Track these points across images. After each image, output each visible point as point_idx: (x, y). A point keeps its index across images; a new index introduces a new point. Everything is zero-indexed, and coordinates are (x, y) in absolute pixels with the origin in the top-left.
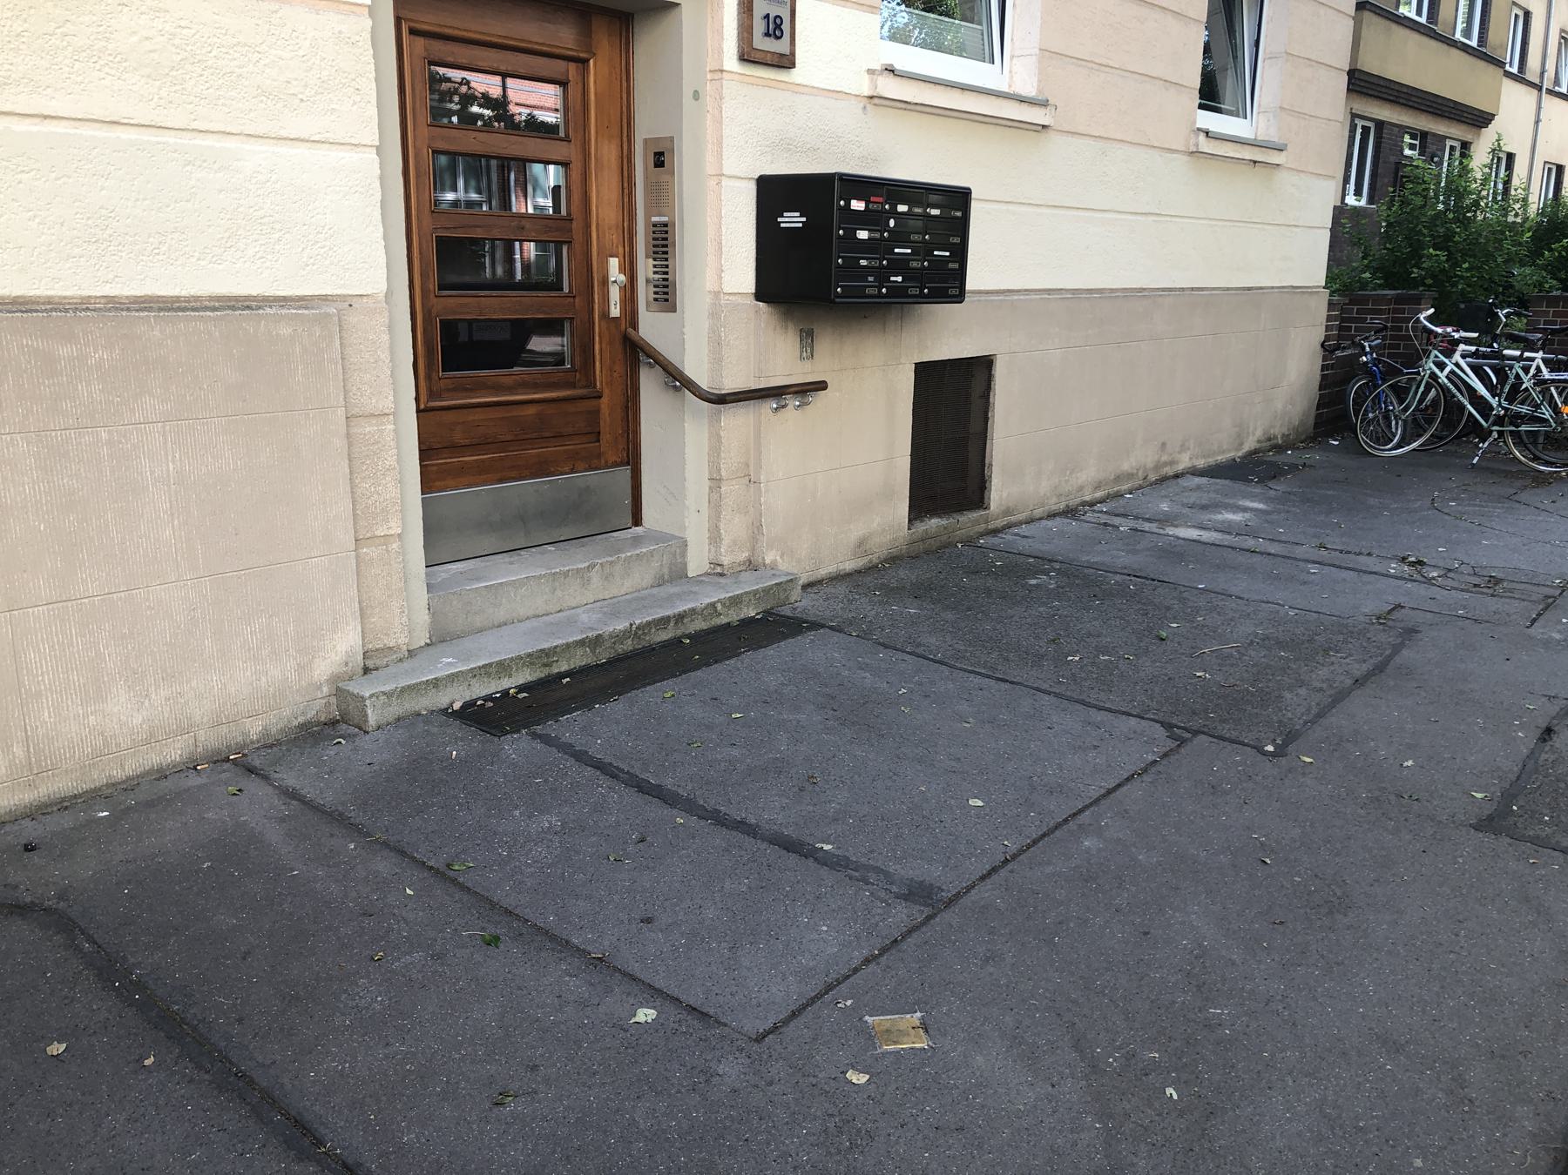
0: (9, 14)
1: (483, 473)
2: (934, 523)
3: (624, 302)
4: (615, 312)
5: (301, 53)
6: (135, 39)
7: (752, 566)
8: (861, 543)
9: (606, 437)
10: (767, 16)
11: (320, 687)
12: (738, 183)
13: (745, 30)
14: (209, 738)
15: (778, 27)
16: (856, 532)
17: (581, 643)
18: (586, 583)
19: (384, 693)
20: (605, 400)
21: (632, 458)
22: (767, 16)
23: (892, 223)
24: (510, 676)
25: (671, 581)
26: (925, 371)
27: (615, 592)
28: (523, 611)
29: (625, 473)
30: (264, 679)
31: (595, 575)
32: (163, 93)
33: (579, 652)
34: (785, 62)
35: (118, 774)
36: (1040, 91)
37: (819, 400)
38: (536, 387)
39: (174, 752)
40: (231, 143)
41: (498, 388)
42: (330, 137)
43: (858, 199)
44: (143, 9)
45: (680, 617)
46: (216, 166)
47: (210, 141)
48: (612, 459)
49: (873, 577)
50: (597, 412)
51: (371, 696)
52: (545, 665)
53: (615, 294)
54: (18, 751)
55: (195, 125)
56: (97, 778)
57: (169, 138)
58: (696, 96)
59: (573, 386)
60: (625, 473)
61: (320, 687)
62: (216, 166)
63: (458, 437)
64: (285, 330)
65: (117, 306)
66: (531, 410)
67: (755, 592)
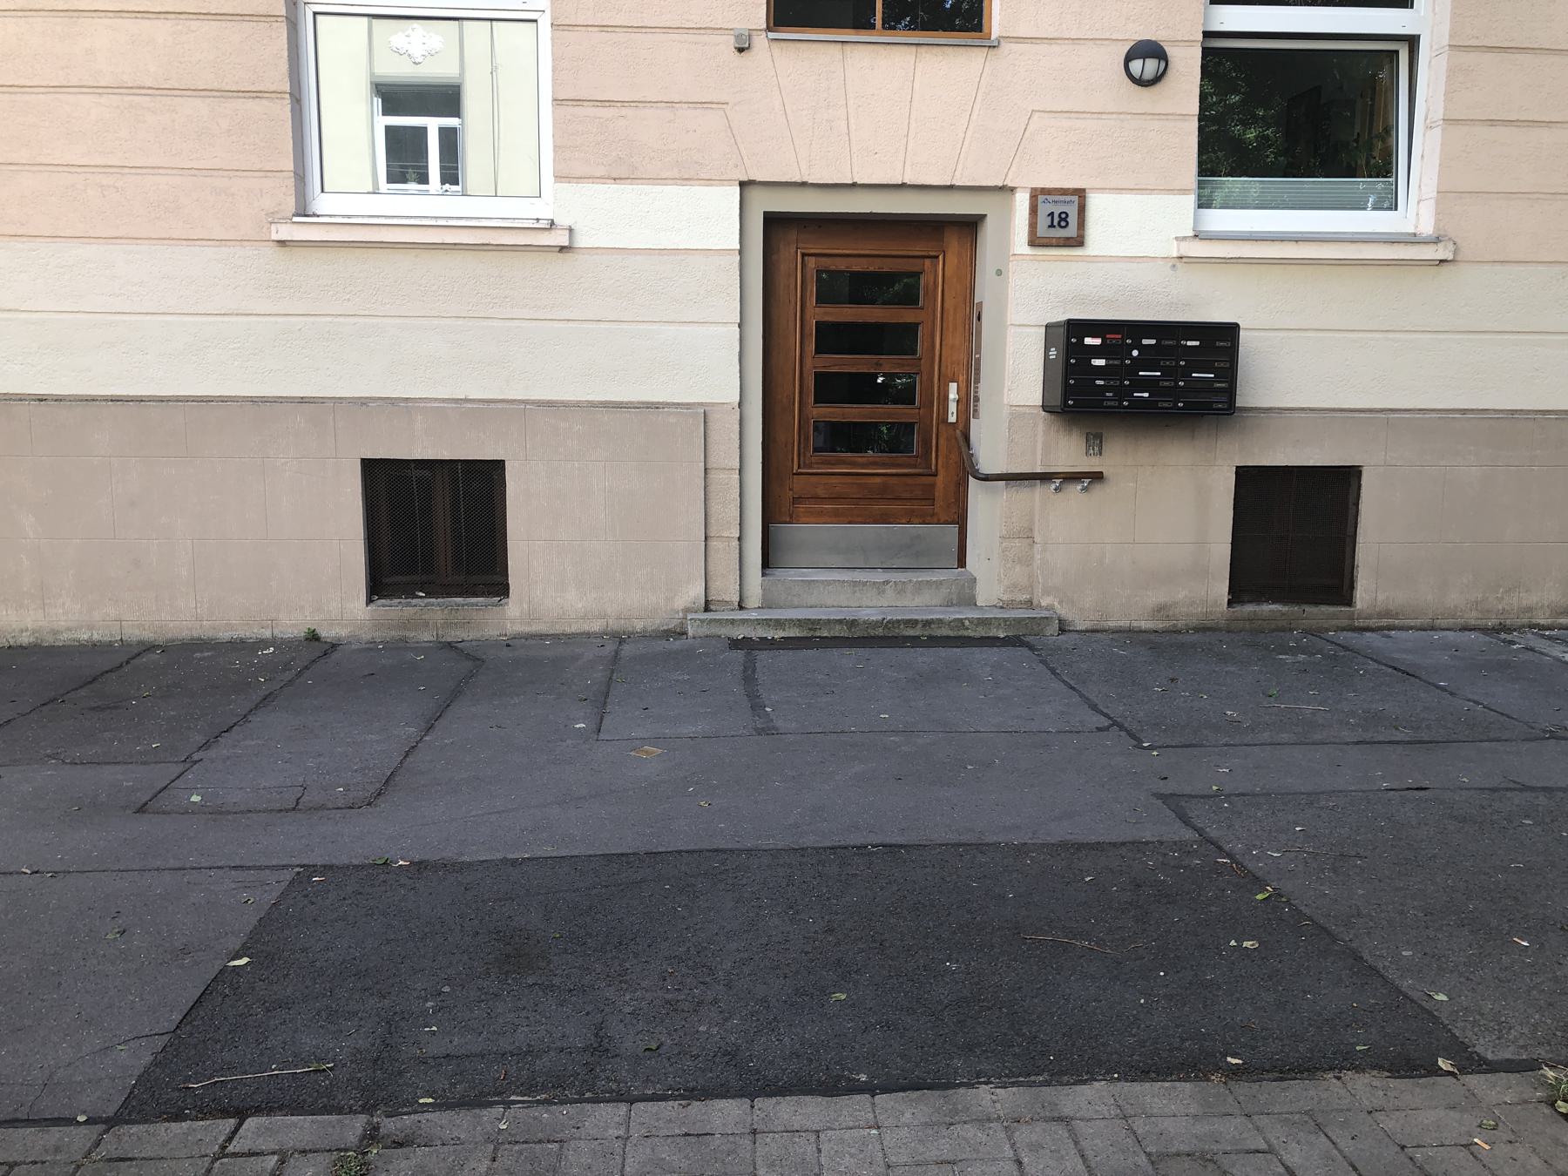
1: (837, 517)
2: (1249, 608)
4: (952, 419)
7: (1029, 604)
8: (1161, 609)
9: (939, 503)
10: (1052, 214)
12: (1033, 330)
13: (1033, 226)
14: (614, 625)
15: (1065, 220)
16: (1155, 597)
17: (840, 622)
18: (881, 592)
20: (940, 479)
21: (961, 520)
22: (1052, 214)
23: (1135, 353)
25: (959, 604)
26: (1243, 474)
27: (906, 603)
28: (829, 603)
29: (954, 529)
31: (889, 590)
34: (1078, 242)
35: (568, 630)
36: (1436, 227)
37: (1099, 491)
38: (884, 465)
39: (596, 626)
40: (655, 327)
41: (853, 464)
45: (927, 623)
47: (644, 326)
48: (943, 518)
49: (1168, 644)
50: (933, 486)
56: (558, 629)
57: (625, 326)
58: (999, 273)
59: (915, 466)
60: (954, 529)
63: (821, 492)
64: (672, 420)
65: (592, 405)
66: (878, 480)
67: (1005, 620)
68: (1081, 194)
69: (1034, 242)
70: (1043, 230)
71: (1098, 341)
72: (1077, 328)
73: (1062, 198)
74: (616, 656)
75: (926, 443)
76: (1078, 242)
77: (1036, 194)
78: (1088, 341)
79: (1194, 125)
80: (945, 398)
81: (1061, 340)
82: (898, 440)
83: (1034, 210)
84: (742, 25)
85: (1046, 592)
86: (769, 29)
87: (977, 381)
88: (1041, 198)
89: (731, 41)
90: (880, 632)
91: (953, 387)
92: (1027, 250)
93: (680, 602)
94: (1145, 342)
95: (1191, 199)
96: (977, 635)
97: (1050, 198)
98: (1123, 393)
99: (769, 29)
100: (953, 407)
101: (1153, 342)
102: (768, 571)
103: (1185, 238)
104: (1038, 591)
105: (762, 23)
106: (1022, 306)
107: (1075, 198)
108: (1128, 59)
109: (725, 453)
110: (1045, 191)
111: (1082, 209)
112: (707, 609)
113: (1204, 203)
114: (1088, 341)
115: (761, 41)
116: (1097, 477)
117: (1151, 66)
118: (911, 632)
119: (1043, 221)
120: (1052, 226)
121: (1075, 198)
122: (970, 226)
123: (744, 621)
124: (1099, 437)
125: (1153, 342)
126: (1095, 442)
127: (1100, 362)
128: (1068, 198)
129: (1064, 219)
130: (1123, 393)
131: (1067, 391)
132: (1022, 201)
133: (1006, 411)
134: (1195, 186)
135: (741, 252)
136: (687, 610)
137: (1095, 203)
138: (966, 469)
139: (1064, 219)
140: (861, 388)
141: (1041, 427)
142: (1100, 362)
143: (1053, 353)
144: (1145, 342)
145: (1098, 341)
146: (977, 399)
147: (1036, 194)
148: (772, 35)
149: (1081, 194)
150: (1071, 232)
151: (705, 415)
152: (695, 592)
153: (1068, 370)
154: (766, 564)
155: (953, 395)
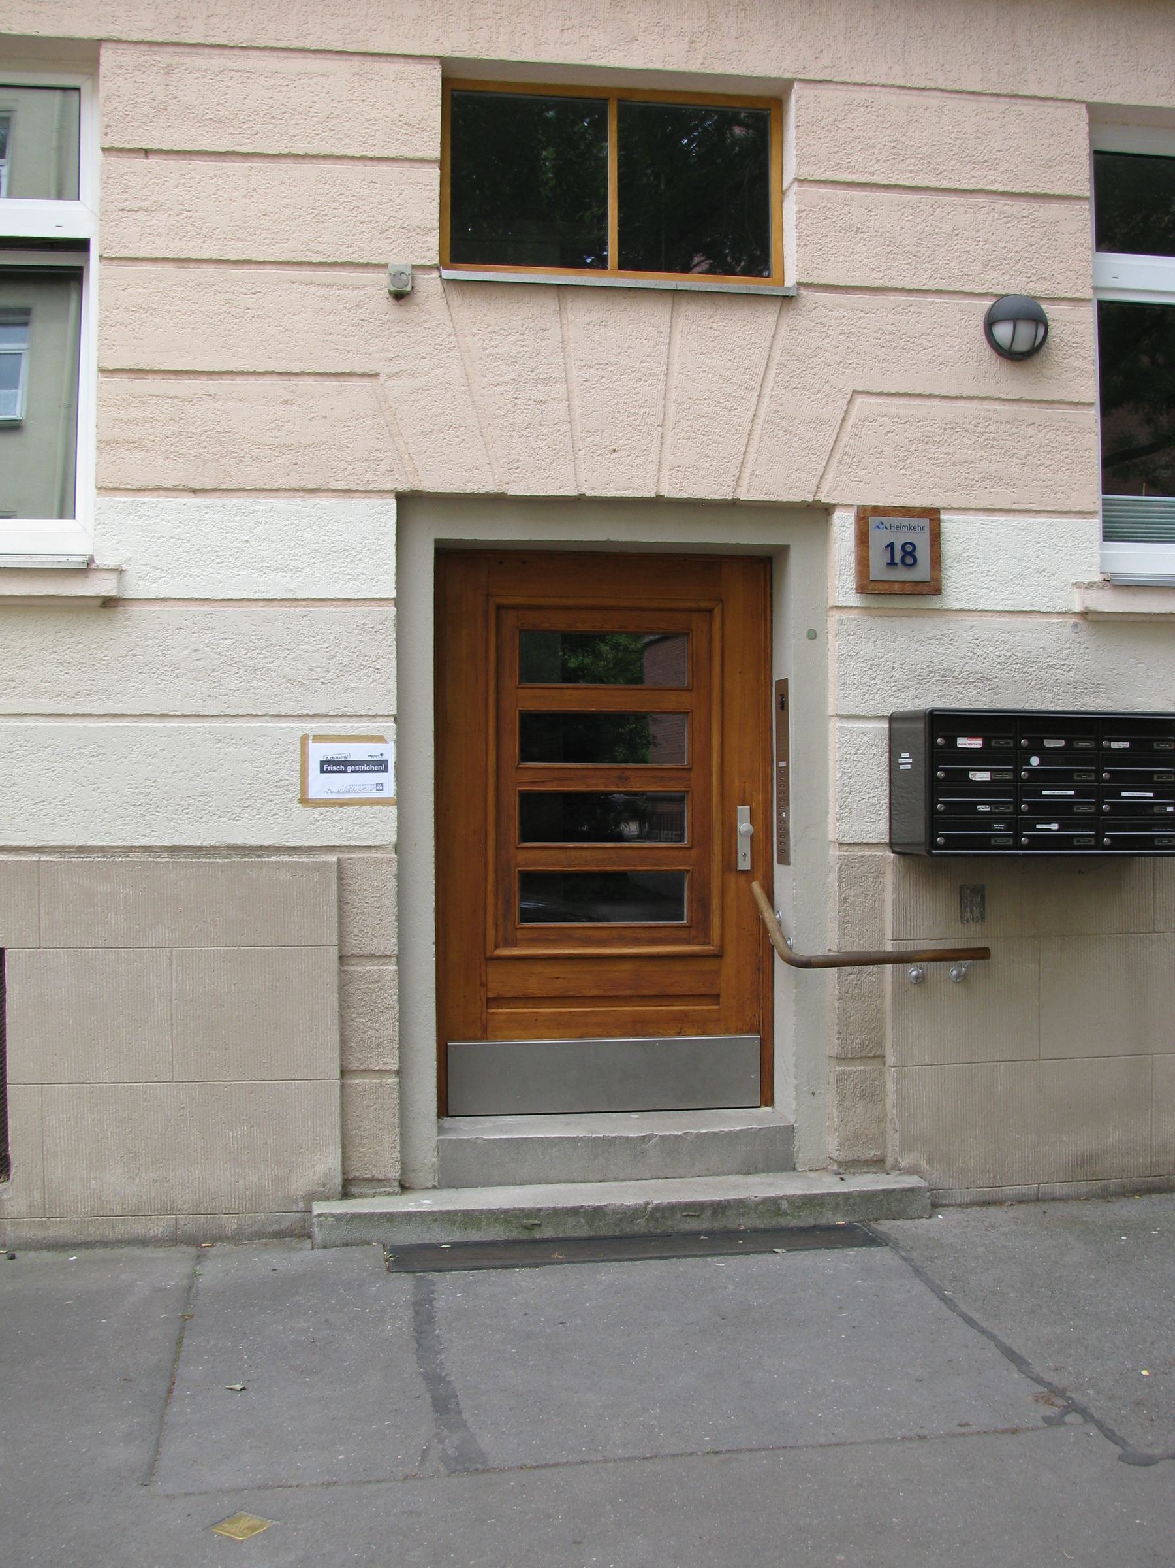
0: (95, 646)
3: (50, 854)
5: (326, 645)
6: (186, 652)
8: (1083, 1161)
10: (891, 545)
11: (296, 1201)
13: (863, 563)
15: (912, 554)
19: (333, 1215)
23: (1035, 761)
24: (479, 1229)
25: (768, 1169)
30: (241, 1182)
32: (203, 690)
33: (571, 1221)
42: (349, 711)
43: (971, 736)
44: (194, 630)
46: (242, 742)
51: (320, 1215)
52: (525, 1227)
53: (744, 847)
54: (37, 1195)
55: (227, 712)
57: (206, 724)
58: (812, 635)
61: (296, 1201)
62: (242, 742)
67: (847, 1196)
68: (932, 514)
69: (867, 586)
70: (878, 569)
71: (977, 743)
72: (945, 724)
73: (906, 521)
74: (189, 1292)
75: (703, 904)
76: (933, 587)
77: (865, 516)
78: (963, 742)
79: (1092, 417)
80: (731, 831)
81: (921, 742)
82: (654, 896)
83: (863, 539)
84: (401, 261)
85: (906, 1145)
86: (442, 265)
87: (784, 802)
88: (873, 521)
89: (381, 282)
90: (641, 1226)
91: (744, 811)
92: (853, 599)
93: (300, 1185)
94: (1049, 743)
95: (1094, 526)
96: (802, 1223)
97: (887, 521)
98: (1017, 825)
99: (442, 265)
100: (744, 847)
101: (1061, 743)
102: (448, 1122)
103: (1089, 586)
104: (893, 1141)
105: (429, 245)
106: (848, 693)
107: (925, 522)
108: (990, 323)
109: (376, 930)
110: (876, 510)
111: (936, 538)
112: (345, 1195)
113: (1111, 534)
114: (963, 742)
115: (429, 284)
116: (982, 954)
117: (1026, 334)
118: (692, 1225)
119: (878, 559)
120: (892, 563)
121: (925, 522)
122: (760, 571)
123: (409, 1216)
124: (979, 892)
125: (1061, 743)
126: (973, 899)
127: (982, 776)
128: (914, 521)
129: (909, 555)
130: (1017, 825)
131: (934, 822)
132: (843, 526)
133: (834, 852)
134: (1098, 507)
135: (398, 602)
136: (312, 1197)
137: (957, 530)
138: (762, 949)
139: (909, 555)
140: (586, 817)
141: (889, 879)
142: (982, 776)
143: (906, 761)
144: (1049, 743)
145: (977, 743)
146: (784, 833)
147: (865, 516)
148: (448, 274)
149: (932, 514)
150: (922, 572)
151: (341, 872)
152: (326, 1164)
153: (934, 789)
154: (444, 1110)
155: (744, 826)
